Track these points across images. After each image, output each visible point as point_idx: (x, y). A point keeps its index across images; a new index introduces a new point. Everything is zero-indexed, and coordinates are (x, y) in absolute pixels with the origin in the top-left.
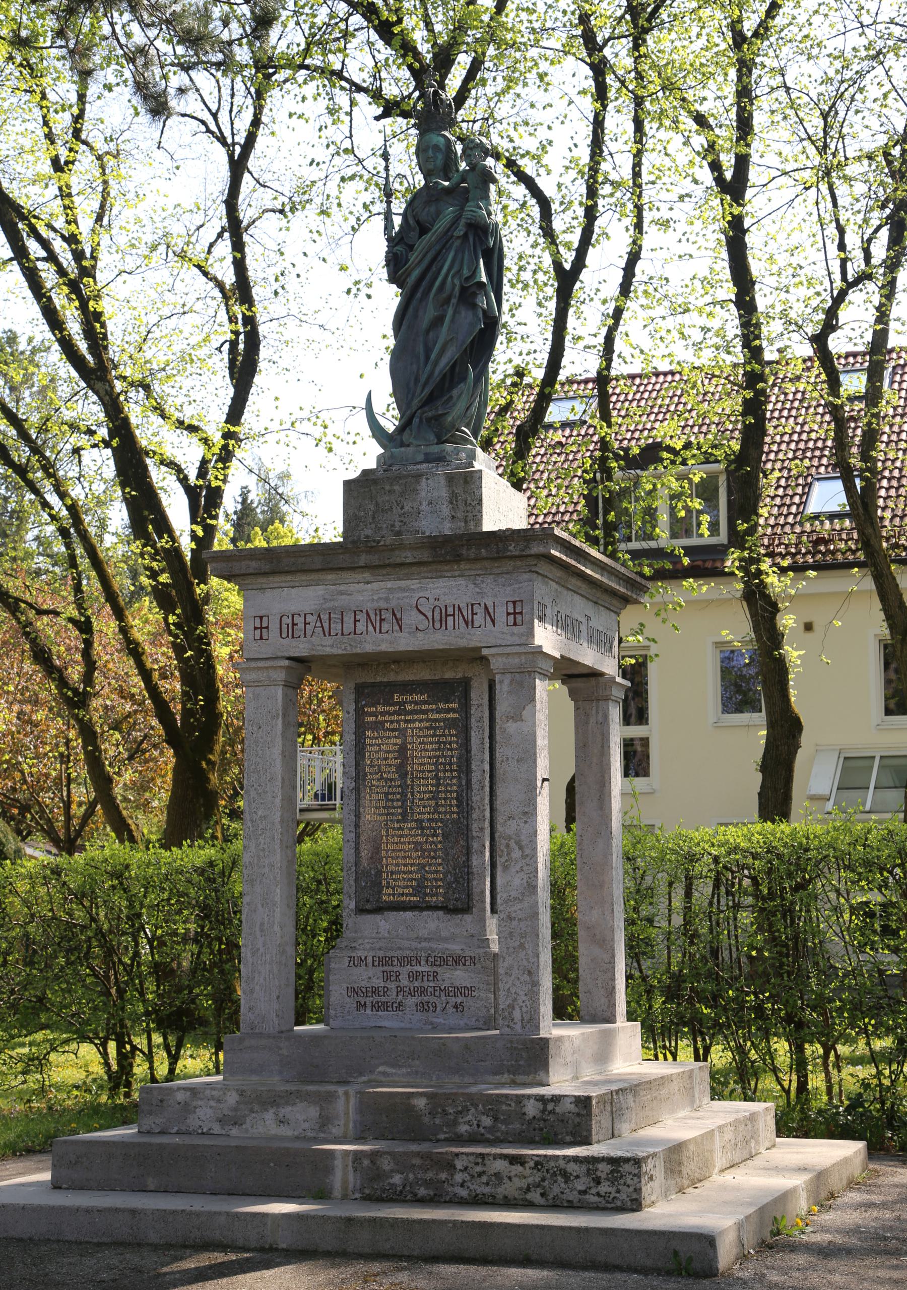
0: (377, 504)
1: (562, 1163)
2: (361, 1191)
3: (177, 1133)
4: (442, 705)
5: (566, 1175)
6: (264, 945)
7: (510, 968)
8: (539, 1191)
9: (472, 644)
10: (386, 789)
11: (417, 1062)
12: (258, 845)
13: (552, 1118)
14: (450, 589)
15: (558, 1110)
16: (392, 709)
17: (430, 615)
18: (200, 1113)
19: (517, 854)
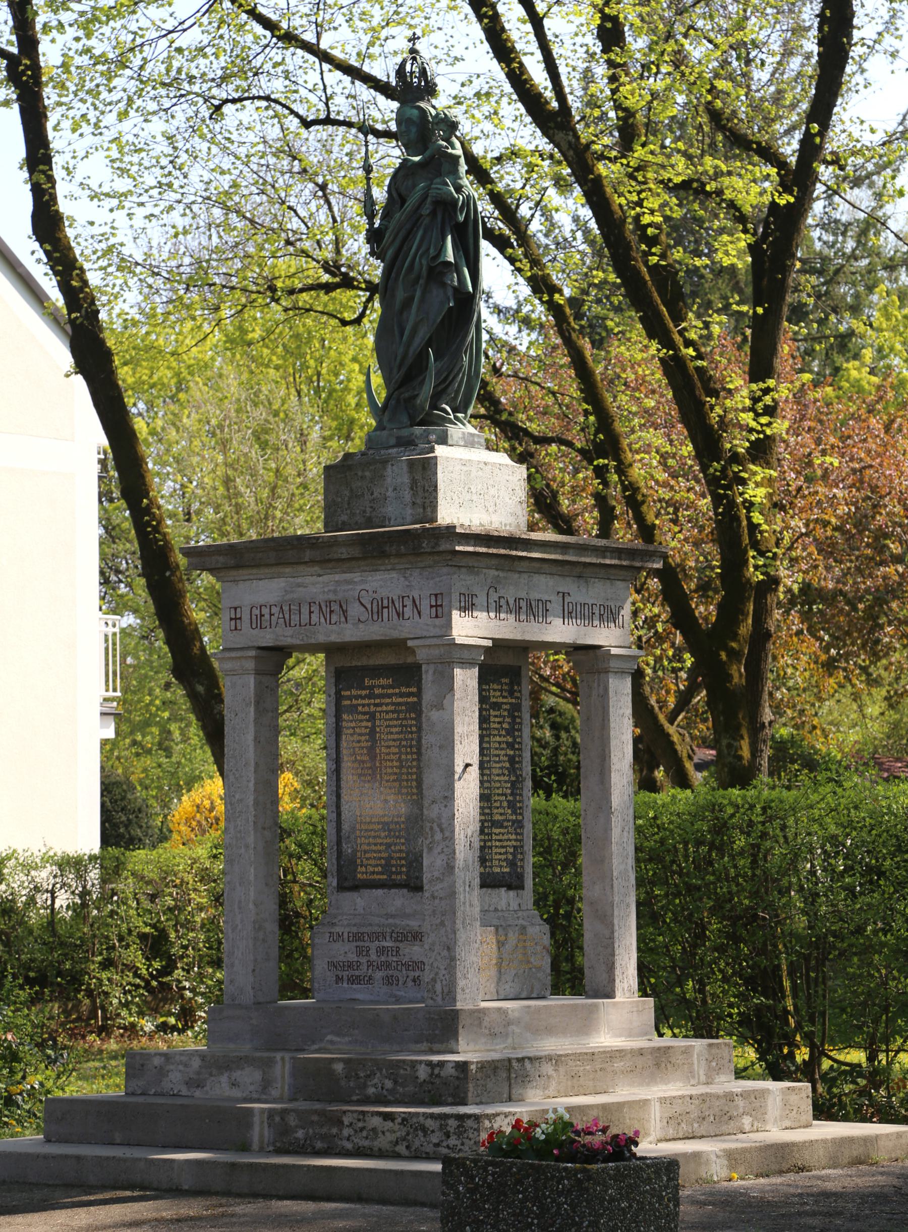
0: (351, 490)
1: (421, 1119)
2: (274, 1144)
3: (154, 1095)
4: (404, 690)
5: (424, 1129)
6: (242, 921)
7: (433, 944)
8: (405, 1144)
9: (404, 635)
10: (359, 771)
11: (356, 1031)
12: (236, 827)
13: (437, 1081)
14: (383, 582)
15: (442, 1074)
16: (364, 693)
17: (369, 607)
18: (172, 1076)
19: (438, 836)
